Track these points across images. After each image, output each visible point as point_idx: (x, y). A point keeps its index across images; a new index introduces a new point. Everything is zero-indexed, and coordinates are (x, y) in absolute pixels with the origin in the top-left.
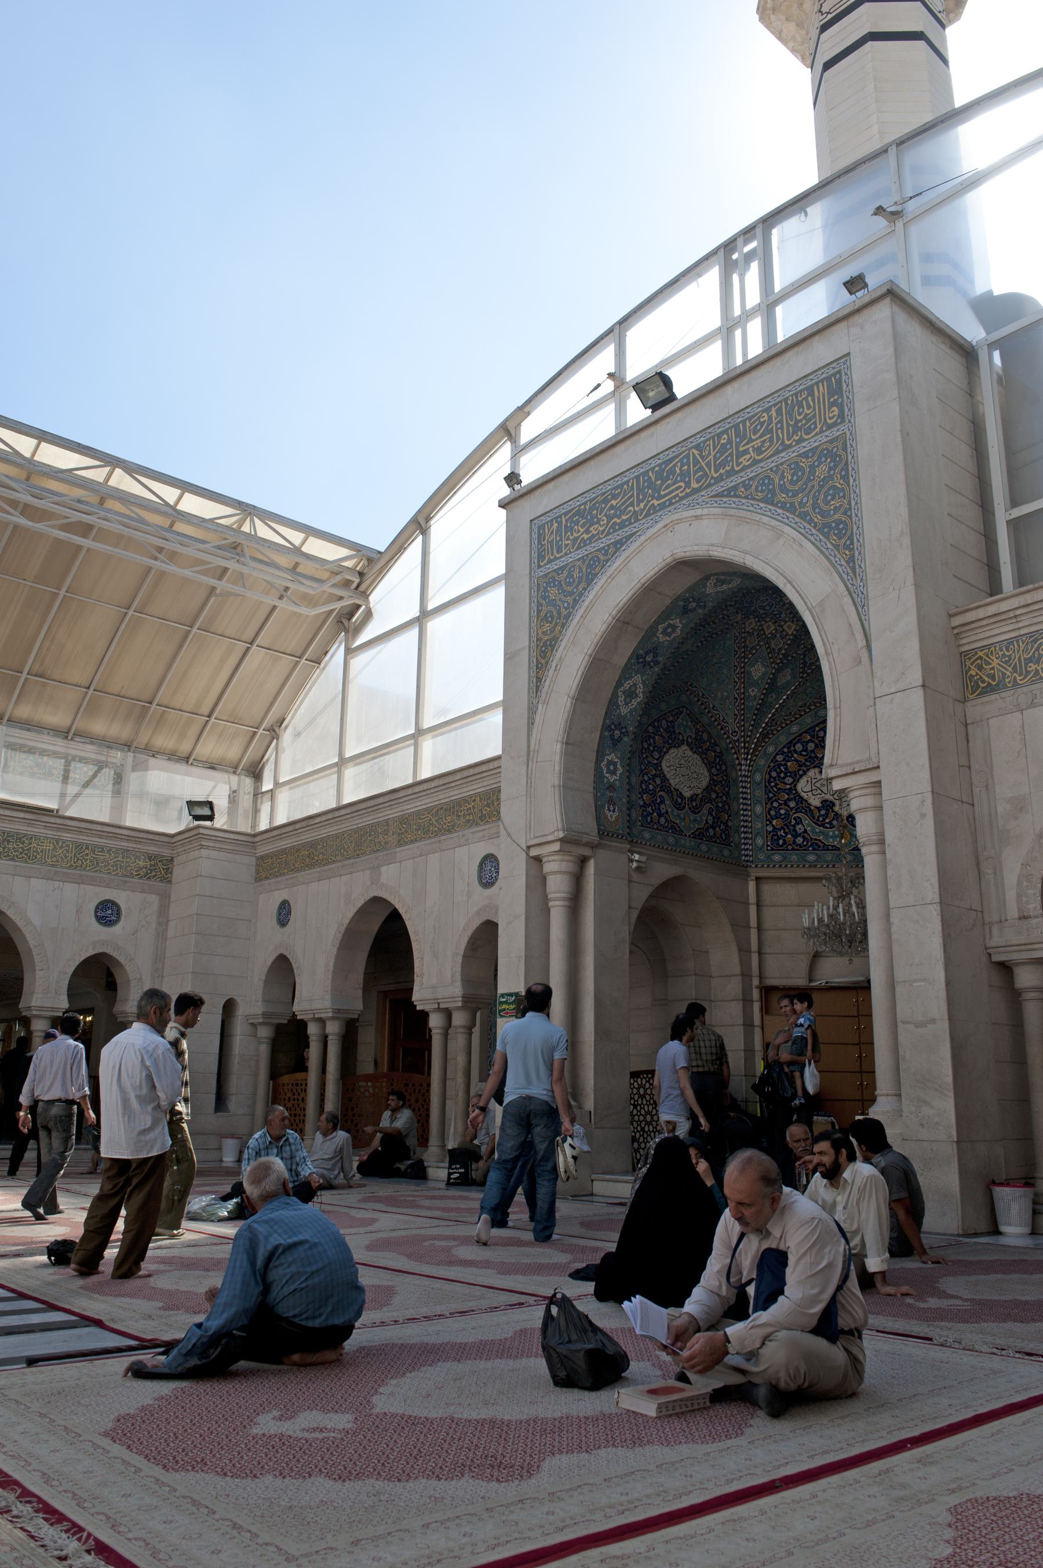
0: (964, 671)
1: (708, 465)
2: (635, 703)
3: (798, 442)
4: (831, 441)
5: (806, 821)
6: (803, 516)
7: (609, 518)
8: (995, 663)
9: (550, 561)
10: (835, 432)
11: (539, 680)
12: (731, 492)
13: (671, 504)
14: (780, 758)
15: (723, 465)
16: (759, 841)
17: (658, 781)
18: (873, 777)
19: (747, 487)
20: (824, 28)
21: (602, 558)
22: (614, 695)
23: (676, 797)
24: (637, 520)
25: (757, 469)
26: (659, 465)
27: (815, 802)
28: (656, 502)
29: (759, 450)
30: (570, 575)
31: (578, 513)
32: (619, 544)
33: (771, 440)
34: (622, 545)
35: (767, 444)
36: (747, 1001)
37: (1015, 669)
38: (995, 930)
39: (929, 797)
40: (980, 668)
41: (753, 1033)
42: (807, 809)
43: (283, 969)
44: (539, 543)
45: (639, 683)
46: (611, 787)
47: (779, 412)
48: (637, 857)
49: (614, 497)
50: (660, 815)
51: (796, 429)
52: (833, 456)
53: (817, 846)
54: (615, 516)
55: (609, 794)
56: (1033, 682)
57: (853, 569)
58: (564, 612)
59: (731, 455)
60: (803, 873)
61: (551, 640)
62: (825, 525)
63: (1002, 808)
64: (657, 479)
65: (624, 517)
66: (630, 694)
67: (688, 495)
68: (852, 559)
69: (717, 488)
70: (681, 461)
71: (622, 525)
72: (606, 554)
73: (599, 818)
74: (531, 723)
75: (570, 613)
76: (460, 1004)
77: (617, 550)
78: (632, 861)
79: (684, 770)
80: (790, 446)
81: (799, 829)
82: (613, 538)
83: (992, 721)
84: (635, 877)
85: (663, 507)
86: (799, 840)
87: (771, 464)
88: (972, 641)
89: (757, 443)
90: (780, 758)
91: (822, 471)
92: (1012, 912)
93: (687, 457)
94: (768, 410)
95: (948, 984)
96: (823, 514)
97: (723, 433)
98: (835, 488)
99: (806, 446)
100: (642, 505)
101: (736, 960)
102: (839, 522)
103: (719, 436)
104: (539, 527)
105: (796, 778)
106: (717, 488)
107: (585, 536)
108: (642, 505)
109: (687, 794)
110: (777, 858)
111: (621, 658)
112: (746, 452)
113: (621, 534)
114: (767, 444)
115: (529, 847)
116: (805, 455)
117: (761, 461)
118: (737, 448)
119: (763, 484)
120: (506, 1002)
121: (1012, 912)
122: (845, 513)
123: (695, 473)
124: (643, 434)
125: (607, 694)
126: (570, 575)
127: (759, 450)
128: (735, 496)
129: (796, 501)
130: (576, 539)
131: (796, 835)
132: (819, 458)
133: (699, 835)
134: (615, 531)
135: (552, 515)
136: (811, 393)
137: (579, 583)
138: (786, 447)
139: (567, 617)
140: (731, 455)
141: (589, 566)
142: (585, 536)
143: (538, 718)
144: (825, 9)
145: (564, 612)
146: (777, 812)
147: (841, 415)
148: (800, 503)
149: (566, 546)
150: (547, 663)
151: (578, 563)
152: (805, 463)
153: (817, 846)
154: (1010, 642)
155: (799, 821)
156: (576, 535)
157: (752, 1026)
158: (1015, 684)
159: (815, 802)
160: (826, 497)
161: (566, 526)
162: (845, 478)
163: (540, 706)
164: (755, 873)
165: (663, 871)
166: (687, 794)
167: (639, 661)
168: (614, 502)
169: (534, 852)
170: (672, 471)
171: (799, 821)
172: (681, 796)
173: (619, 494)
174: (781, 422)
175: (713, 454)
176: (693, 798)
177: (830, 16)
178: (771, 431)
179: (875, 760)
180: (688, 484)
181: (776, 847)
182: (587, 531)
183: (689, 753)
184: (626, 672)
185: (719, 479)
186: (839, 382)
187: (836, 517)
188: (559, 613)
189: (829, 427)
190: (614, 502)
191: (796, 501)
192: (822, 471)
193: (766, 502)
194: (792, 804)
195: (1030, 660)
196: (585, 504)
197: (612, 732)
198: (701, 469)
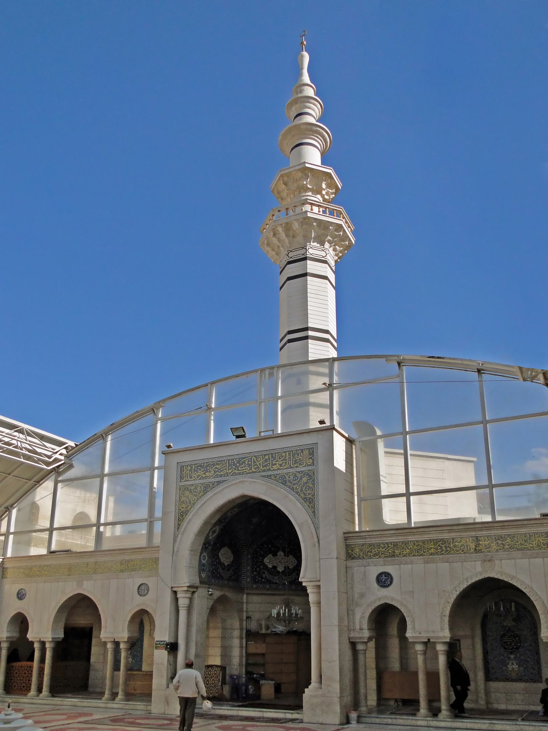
0: (347, 550)
1: (260, 464)
2: (215, 535)
3: (297, 467)
4: (309, 470)
5: (266, 573)
6: (297, 493)
7: (215, 472)
8: (357, 550)
9: (186, 481)
10: (310, 468)
11: (179, 525)
12: (269, 477)
13: (243, 474)
14: (258, 549)
15: (266, 466)
16: (249, 580)
17: (217, 561)
18: (318, 583)
19: (275, 477)
20: (289, 263)
21: (211, 485)
22: (209, 533)
23: (222, 564)
24: (227, 476)
25: (280, 472)
26: (239, 458)
27: (270, 566)
28: (236, 472)
29: (281, 465)
30: (196, 488)
31: (200, 466)
32: (219, 483)
33: (286, 463)
34: (221, 483)
35: (284, 464)
36: (241, 638)
37: (363, 553)
38: (352, 632)
39: (337, 594)
40: (352, 551)
41: (242, 650)
42: (266, 567)
43: (21, 622)
44: (181, 472)
45: (217, 528)
46: (204, 565)
47: (289, 454)
48: (211, 590)
49: (217, 464)
50: (218, 573)
51: (296, 462)
52: (310, 476)
53: (269, 582)
54: (218, 471)
55: (203, 567)
56: (369, 559)
57: (315, 515)
58: (192, 502)
59: (269, 463)
60: (265, 592)
61: (186, 511)
62: (305, 498)
63: (356, 595)
64: (237, 463)
65: (222, 473)
66: (214, 532)
67: (250, 473)
68: (314, 512)
69: (264, 474)
70: (248, 459)
71: (221, 476)
72: (213, 484)
73: (200, 577)
74: (175, 541)
75: (195, 503)
76: (126, 640)
77: (218, 484)
78: (209, 591)
79: (226, 556)
80: (293, 468)
81: (264, 576)
82: (217, 479)
83: (355, 568)
84: (209, 597)
85: (239, 474)
86: (263, 580)
87: (285, 471)
88: (351, 542)
89: (281, 463)
90: (258, 549)
91: (305, 479)
92: (358, 627)
93: (251, 459)
94: (285, 452)
95: (339, 650)
96: (304, 494)
97: (267, 455)
98: (309, 486)
99: (299, 469)
100: (230, 471)
101: (238, 623)
102: (310, 498)
103: (265, 455)
104: (181, 466)
105: (264, 557)
106: (264, 474)
107: (204, 476)
108: (230, 471)
109: (226, 564)
110: (255, 586)
111: (213, 521)
112: (275, 464)
113: (220, 479)
114: (284, 464)
115: (172, 587)
116: (299, 472)
117: (280, 469)
118: (272, 462)
119: (282, 478)
120: (159, 644)
121: (358, 627)
122: (312, 496)
123: (254, 466)
124: (232, 445)
125: (207, 532)
126: (196, 488)
127: (281, 465)
128: (270, 478)
129: (295, 487)
130: (199, 476)
131: (262, 578)
132: (304, 475)
133: (229, 579)
134: (217, 477)
135: (188, 463)
136: (302, 452)
137: (200, 492)
138: (291, 468)
139: (194, 504)
140: (269, 463)
141: (205, 487)
142: (204, 476)
143: (178, 540)
144: (290, 255)
145: (192, 502)
146: (256, 569)
147: (313, 463)
148: (296, 488)
149: (194, 477)
150: (183, 519)
151: (200, 485)
152: (299, 475)
153: (269, 582)
154: (363, 545)
155: (264, 573)
156: (199, 474)
157: (242, 647)
158: (363, 558)
159: (270, 566)
160: (306, 488)
161: (194, 470)
162: (313, 484)
163: (180, 535)
164: (246, 591)
165: (217, 594)
166: (226, 564)
167: (219, 521)
168: (218, 467)
169: (174, 589)
170: (244, 462)
171: (264, 573)
172: (224, 565)
173: (220, 464)
174: (290, 458)
175: (262, 461)
176: (228, 565)
177: (292, 259)
178: (286, 460)
179: (319, 578)
180: (251, 469)
181: (255, 582)
182: (204, 474)
183: (227, 549)
184: (215, 524)
185: (264, 471)
186: (313, 451)
187: (309, 496)
188: (190, 502)
189: (308, 465)
190: (218, 467)
191: (295, 487)
192: (305, 479)
193: (283, 484)
194: (261, 567)
195: (368, 552)
196: (204, 463)
197: (206, 545)
198: (257, 465)
